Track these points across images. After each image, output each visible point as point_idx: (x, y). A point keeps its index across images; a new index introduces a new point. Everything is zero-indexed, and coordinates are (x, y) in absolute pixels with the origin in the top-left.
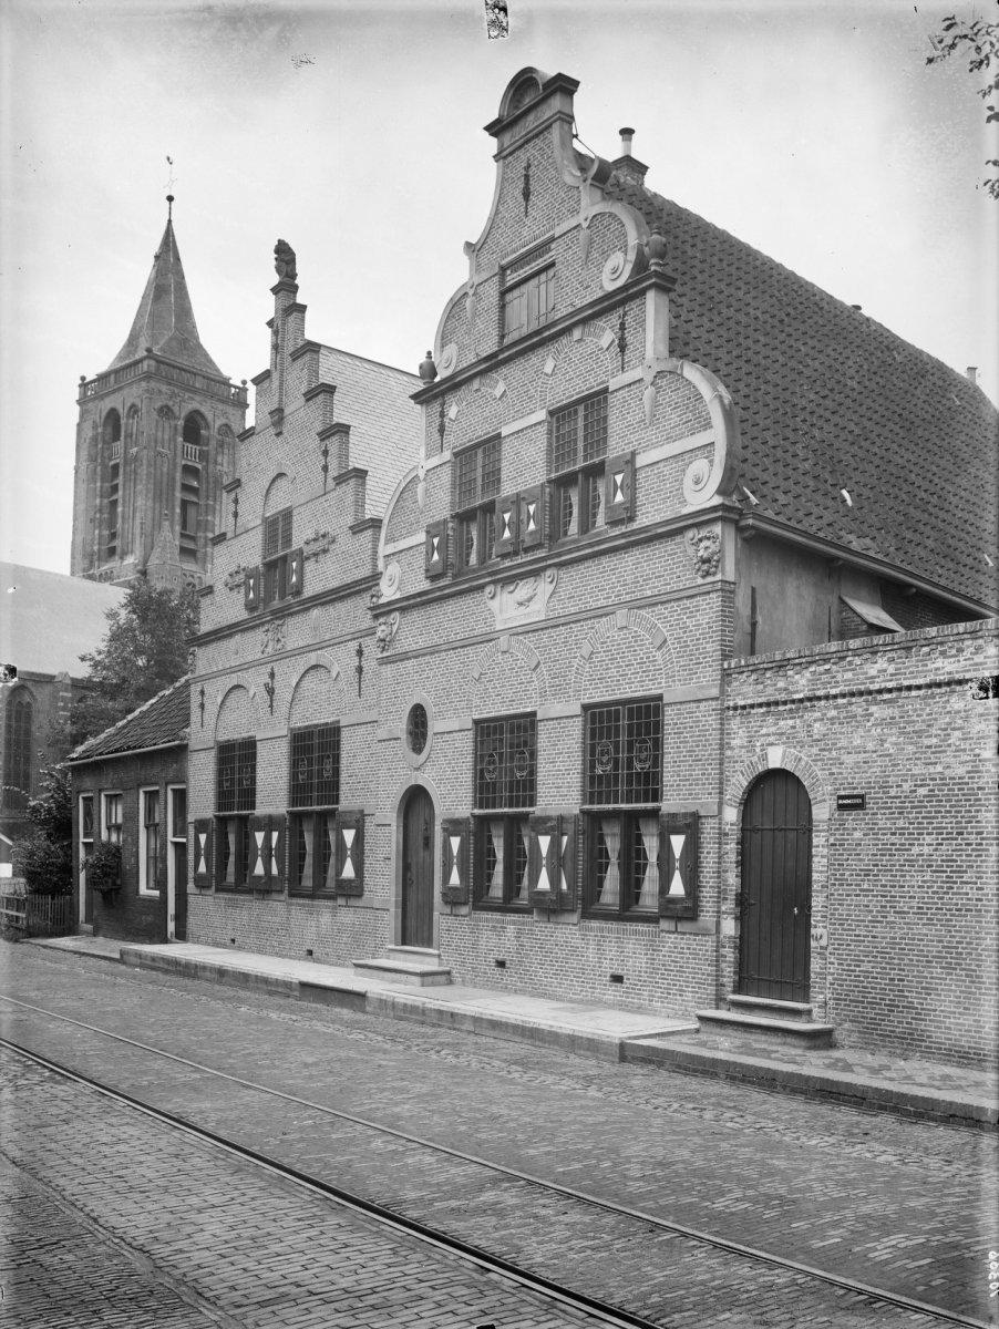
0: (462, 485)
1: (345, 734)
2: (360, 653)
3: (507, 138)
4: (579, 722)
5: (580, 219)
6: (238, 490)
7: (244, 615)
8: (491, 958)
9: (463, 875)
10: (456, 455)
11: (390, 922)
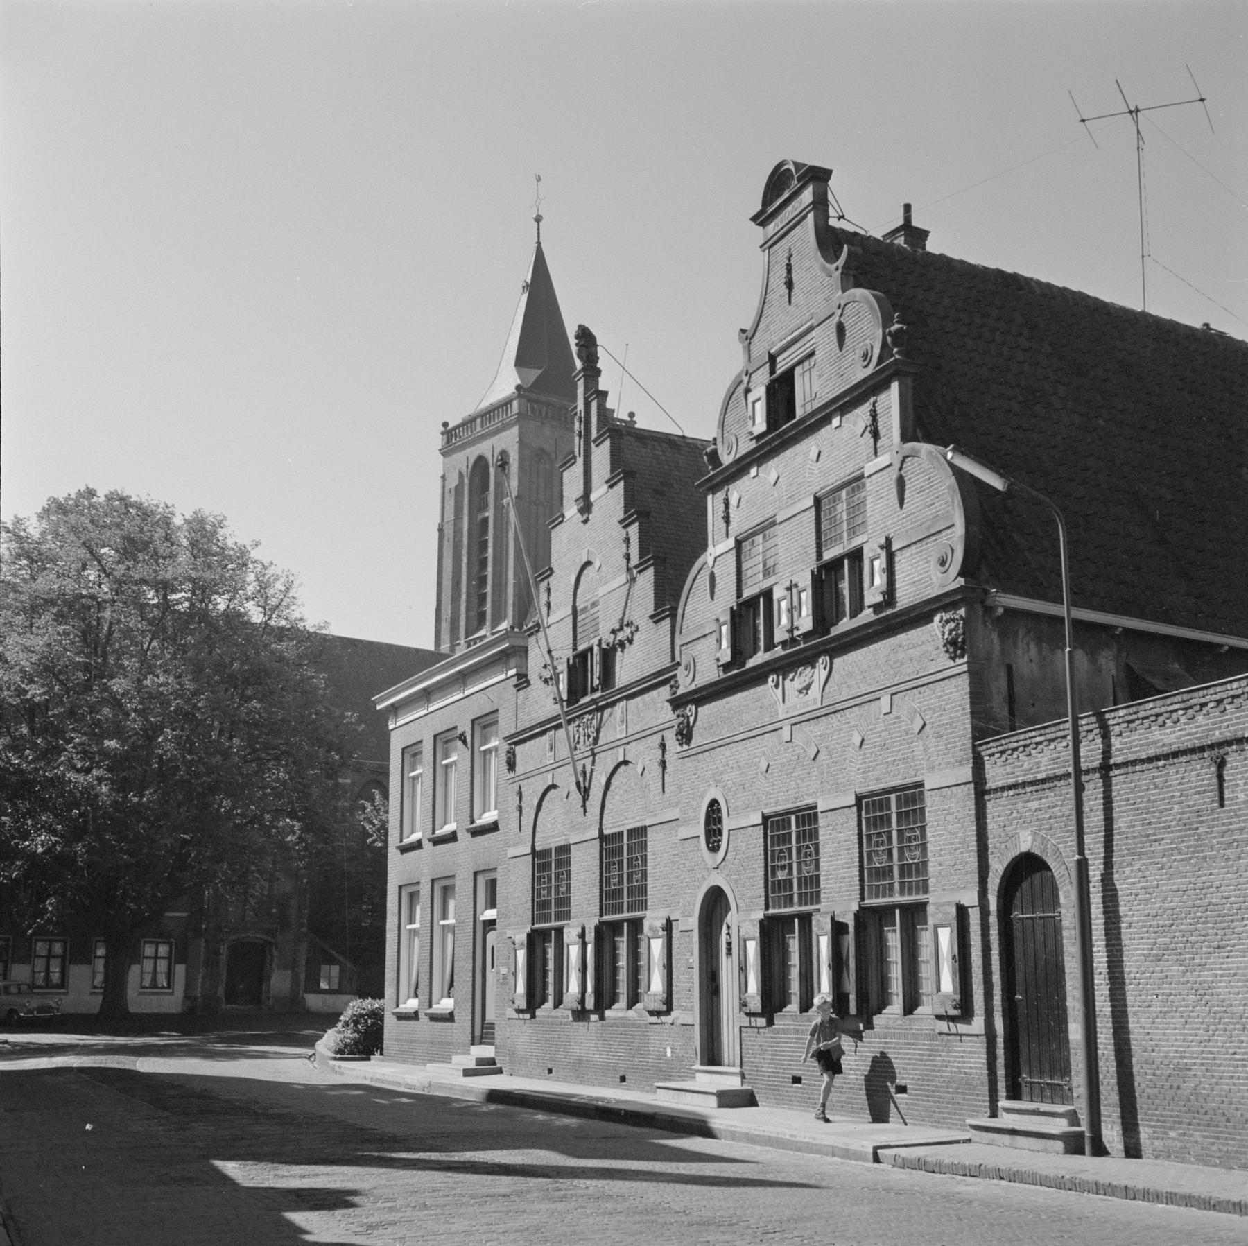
2: (663, 746)
3: (772, 228)
6: (550, 579)
7: (556, 709)
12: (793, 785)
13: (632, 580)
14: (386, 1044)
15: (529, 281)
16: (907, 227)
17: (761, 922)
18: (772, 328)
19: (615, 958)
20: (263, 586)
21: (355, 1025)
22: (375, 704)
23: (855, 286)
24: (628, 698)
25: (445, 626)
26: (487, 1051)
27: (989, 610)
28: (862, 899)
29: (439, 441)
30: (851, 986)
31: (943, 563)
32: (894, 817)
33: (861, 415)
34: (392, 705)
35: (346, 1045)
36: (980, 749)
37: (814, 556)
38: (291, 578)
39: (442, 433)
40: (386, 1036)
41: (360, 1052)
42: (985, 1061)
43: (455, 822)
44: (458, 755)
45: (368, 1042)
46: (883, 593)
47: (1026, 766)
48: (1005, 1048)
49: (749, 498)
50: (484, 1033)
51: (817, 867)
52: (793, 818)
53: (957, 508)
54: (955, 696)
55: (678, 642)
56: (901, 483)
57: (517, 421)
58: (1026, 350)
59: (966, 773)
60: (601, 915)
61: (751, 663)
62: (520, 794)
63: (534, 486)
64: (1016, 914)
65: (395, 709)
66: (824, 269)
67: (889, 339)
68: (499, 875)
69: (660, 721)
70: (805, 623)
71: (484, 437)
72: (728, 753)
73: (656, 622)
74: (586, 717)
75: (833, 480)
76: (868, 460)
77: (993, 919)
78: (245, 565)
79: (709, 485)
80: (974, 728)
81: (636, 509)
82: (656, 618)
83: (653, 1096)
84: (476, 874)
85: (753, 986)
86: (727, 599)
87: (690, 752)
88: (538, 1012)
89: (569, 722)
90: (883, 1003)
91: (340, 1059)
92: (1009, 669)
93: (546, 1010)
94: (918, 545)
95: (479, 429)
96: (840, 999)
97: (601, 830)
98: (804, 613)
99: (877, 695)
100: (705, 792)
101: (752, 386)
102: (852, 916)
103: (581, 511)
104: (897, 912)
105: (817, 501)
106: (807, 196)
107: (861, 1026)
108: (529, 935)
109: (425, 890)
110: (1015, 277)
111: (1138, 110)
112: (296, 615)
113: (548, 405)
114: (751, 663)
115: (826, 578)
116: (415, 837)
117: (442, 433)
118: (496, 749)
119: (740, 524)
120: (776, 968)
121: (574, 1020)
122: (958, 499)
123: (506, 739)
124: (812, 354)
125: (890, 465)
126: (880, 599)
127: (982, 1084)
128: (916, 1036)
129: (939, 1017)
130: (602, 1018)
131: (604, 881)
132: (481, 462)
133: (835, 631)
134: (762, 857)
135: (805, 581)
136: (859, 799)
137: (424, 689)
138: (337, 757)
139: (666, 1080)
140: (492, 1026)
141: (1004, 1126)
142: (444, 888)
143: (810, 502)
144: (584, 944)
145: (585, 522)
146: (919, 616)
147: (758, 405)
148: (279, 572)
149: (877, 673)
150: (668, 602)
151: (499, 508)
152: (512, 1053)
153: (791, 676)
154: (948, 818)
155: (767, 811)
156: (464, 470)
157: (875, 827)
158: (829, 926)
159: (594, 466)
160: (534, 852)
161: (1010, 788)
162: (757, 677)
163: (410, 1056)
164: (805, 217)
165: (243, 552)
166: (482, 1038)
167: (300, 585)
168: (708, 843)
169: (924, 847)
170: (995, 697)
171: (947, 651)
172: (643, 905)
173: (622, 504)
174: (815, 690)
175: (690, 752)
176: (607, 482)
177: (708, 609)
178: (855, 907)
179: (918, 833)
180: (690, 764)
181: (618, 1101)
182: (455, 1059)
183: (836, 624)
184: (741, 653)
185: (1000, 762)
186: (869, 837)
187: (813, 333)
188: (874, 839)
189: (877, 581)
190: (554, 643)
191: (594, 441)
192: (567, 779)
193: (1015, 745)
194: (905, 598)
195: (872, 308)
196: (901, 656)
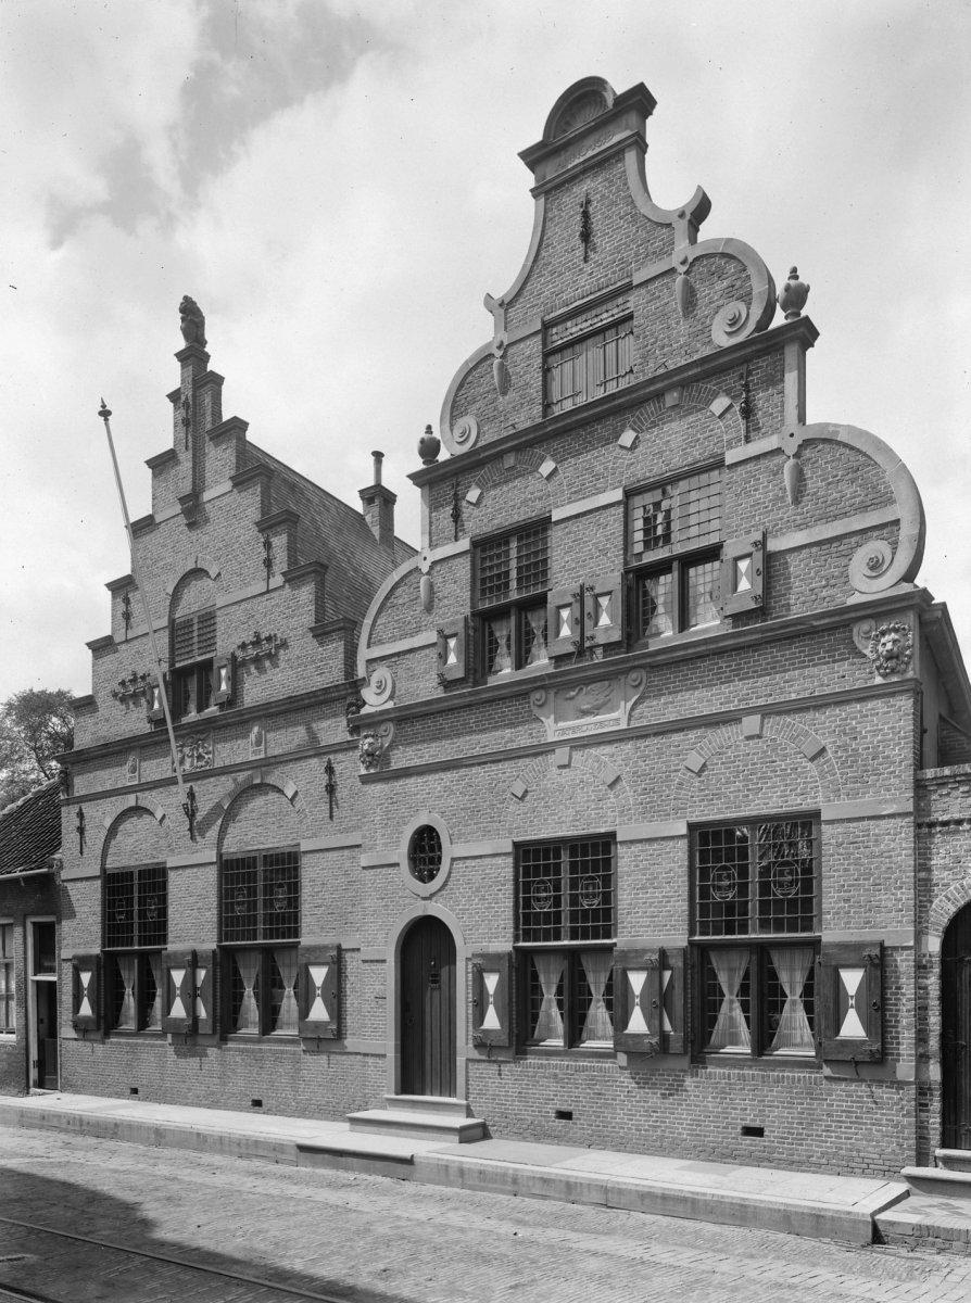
0: (486, 579)
1: (305, 861)
3: (551, 171)
4: (683, 844)
5: (674, 261)
8: (551, 1109)
9: (95, 1005)
10: (475, 544)
11: (387, 1070)
189: (744, 585)
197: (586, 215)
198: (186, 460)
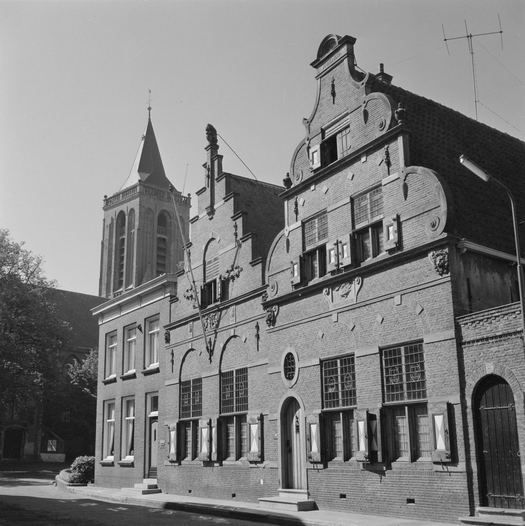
2: (257, 327)
3: (322, 69)
6: (190, 248)
12: (339, 344)
13: (240, 246)
14: (96, 477)
15: (145, 135)
16: (382, 73)
17: (320, 415)
18: (323, 116)
19: (228, 435)
20: (26, 262)
21: (79, 469)
22: (92, 312)
23: (372, 92)
24: (237, 304)
25: (104, 287)
26: (153, 482)
27: (459, 250)
28: (384, 401)
29: (102, 204)
30: (378, 447)
31: (433, 226)
32: (403, 359)
33: (379, 155)
34: (101, 313)
35: (75, 479)
36: (459, 321)
37: (351, 227)
38: (40, 259)
39: (104, 200)
40: (96, 474)
41: (81, 482)
42: (466, 486)
43: (135, 368)
44: (137, 337)
45: (86, 477)
46: (396, 243)
47: (488, 329)
48: (478, 479)
49: (309, 202)
50: (150, 472)
51: (354, 386)
52: (339, 361)
53: (442, 198)
54: (443, 293)
55: (267, 274)
56: (406, 188)
57: (139, 196)
58: (443, 133)
59: (451, 333)
60: (220, 413)
61: (311, 284)
62: (173, 354)
63: (145, 225)
64: (483, 407)
65: (102, 315)
66: (355, 85)
67: (396, 115)
68: (159, 395)
69: (255, 315)
70: (347, 260)
71: (123, 203)
72: (298, 329)
73: (253, 266)
74: (212, 314)
75: (362, 188)
76: (384, 177)
77: (469, 410)
78: (18, 253)
79: (286, 196)
80: (455, 310)
81: (239, 211)
82: (253, 264)
83: (258, 505)
84: (146, 394)
85: (315, 448)
86: (296, 251)
87: (275, 330)
88: (183, 462)
89: (204, 316)
90: (397, 455)
91: (72, 486)
92: (468, 280)
93: (187, 461)
94: (417, 218)
95: (121, 198)
96: (372, 455)
97: (220, 371)
98: (346, 255)
99: (392, 295)
100: (284, 349)
101: (311, 145)
102: (378, 411)
103: (209, 214)
104: (406, 408)
105: (352, 200)
106: (344, 51)
107: (385, 468)
108: (178, 424)
109: (118, 402)
110: (431, 101)
111: (471, 36)
112: (41, 276)
113: (152, 189)
114: (311, 284)
115: (357, 238)
116: (132, 372)
117: (104, 200)
118: (158, 333)
119: (304, 214)
120: (328, 438)
121: (205, 466)
122: (442, 193)
123: (164, 327)
124: (348, 126)
125: (399, 178)
126: (394, 246)
127: (465, 498)
128: (421, 473)
129: (435, 463)
130: (221, 465)
131: (222, 396)
132: (122, 213)
133: (363, 265)
134: (320, 381)
135: (346, 239)
136: (381, 350)
137: (119, 305)
138: (61, 342)
139: (270, 495)
140: (155, 469)
141: (477, 521)
142: (129, 402)
143: (348, 200)
144: (211, 428)
145: (211, 219)
146: (419, 253)
147: (315, 154)
148: (34, 256)
149: (391, 285)
150: (260, 256)
151: (130, 234)
152: (167, 483)
153: (337, 288)
154: (439, 358)
155: (322, 358)
156: (114, 217)
157: (329, 375)
158: (365, 416)
159: (216, 192)
160: (180, 382)
161: (478, 341)
162: (317, 289)
163: (109, 483)
164: (342, 61)
165: (17, 247)
166: (149, 475)
167: (44, 262)
168: (286, 375)
169: (423, 374)
170: (463, 295)
171: (438, 271)
172: (246, 408)
173: (233, 209)
174: (352, 295)
175: (275, 330)
176: (224, 199)
177: (285, 258)
178: (380, 406)
179: (419, 366)
180: (274, 336)
181: (241, 508)
182: (136, 485)
183: (364, 261)
184: (305, 279)
185: (471, 328)
186: (387, 370)
187: (348, 117)
188: (390, 370)
189: (392, 237)
190: (189, 282)
191: (216, 179)
192: (201, 346)
193: (482, 318)
194: (408, 245)
195: (385, 101)
196: (406, 275)
197: (333, 86)
198: (208, 190)
